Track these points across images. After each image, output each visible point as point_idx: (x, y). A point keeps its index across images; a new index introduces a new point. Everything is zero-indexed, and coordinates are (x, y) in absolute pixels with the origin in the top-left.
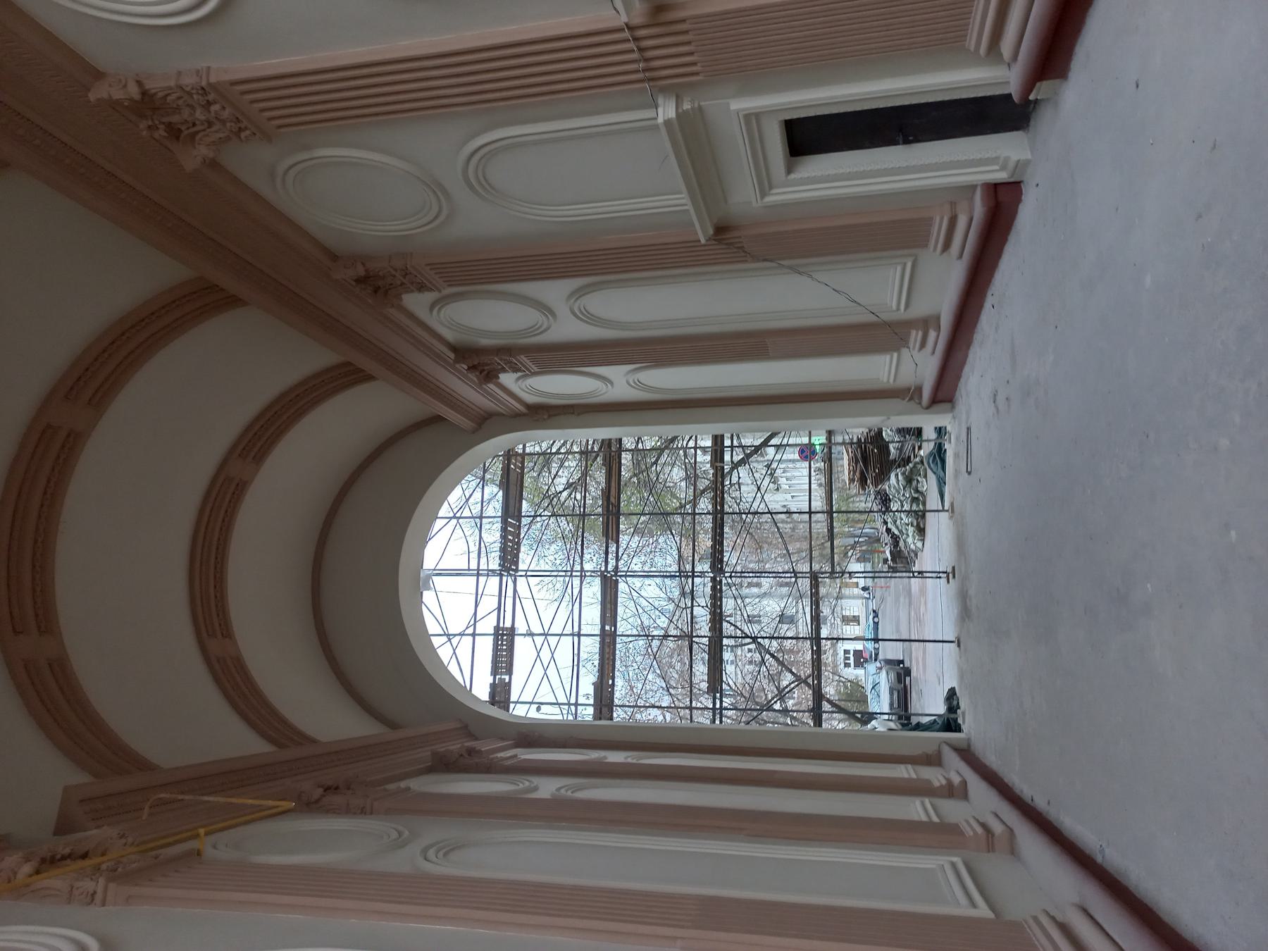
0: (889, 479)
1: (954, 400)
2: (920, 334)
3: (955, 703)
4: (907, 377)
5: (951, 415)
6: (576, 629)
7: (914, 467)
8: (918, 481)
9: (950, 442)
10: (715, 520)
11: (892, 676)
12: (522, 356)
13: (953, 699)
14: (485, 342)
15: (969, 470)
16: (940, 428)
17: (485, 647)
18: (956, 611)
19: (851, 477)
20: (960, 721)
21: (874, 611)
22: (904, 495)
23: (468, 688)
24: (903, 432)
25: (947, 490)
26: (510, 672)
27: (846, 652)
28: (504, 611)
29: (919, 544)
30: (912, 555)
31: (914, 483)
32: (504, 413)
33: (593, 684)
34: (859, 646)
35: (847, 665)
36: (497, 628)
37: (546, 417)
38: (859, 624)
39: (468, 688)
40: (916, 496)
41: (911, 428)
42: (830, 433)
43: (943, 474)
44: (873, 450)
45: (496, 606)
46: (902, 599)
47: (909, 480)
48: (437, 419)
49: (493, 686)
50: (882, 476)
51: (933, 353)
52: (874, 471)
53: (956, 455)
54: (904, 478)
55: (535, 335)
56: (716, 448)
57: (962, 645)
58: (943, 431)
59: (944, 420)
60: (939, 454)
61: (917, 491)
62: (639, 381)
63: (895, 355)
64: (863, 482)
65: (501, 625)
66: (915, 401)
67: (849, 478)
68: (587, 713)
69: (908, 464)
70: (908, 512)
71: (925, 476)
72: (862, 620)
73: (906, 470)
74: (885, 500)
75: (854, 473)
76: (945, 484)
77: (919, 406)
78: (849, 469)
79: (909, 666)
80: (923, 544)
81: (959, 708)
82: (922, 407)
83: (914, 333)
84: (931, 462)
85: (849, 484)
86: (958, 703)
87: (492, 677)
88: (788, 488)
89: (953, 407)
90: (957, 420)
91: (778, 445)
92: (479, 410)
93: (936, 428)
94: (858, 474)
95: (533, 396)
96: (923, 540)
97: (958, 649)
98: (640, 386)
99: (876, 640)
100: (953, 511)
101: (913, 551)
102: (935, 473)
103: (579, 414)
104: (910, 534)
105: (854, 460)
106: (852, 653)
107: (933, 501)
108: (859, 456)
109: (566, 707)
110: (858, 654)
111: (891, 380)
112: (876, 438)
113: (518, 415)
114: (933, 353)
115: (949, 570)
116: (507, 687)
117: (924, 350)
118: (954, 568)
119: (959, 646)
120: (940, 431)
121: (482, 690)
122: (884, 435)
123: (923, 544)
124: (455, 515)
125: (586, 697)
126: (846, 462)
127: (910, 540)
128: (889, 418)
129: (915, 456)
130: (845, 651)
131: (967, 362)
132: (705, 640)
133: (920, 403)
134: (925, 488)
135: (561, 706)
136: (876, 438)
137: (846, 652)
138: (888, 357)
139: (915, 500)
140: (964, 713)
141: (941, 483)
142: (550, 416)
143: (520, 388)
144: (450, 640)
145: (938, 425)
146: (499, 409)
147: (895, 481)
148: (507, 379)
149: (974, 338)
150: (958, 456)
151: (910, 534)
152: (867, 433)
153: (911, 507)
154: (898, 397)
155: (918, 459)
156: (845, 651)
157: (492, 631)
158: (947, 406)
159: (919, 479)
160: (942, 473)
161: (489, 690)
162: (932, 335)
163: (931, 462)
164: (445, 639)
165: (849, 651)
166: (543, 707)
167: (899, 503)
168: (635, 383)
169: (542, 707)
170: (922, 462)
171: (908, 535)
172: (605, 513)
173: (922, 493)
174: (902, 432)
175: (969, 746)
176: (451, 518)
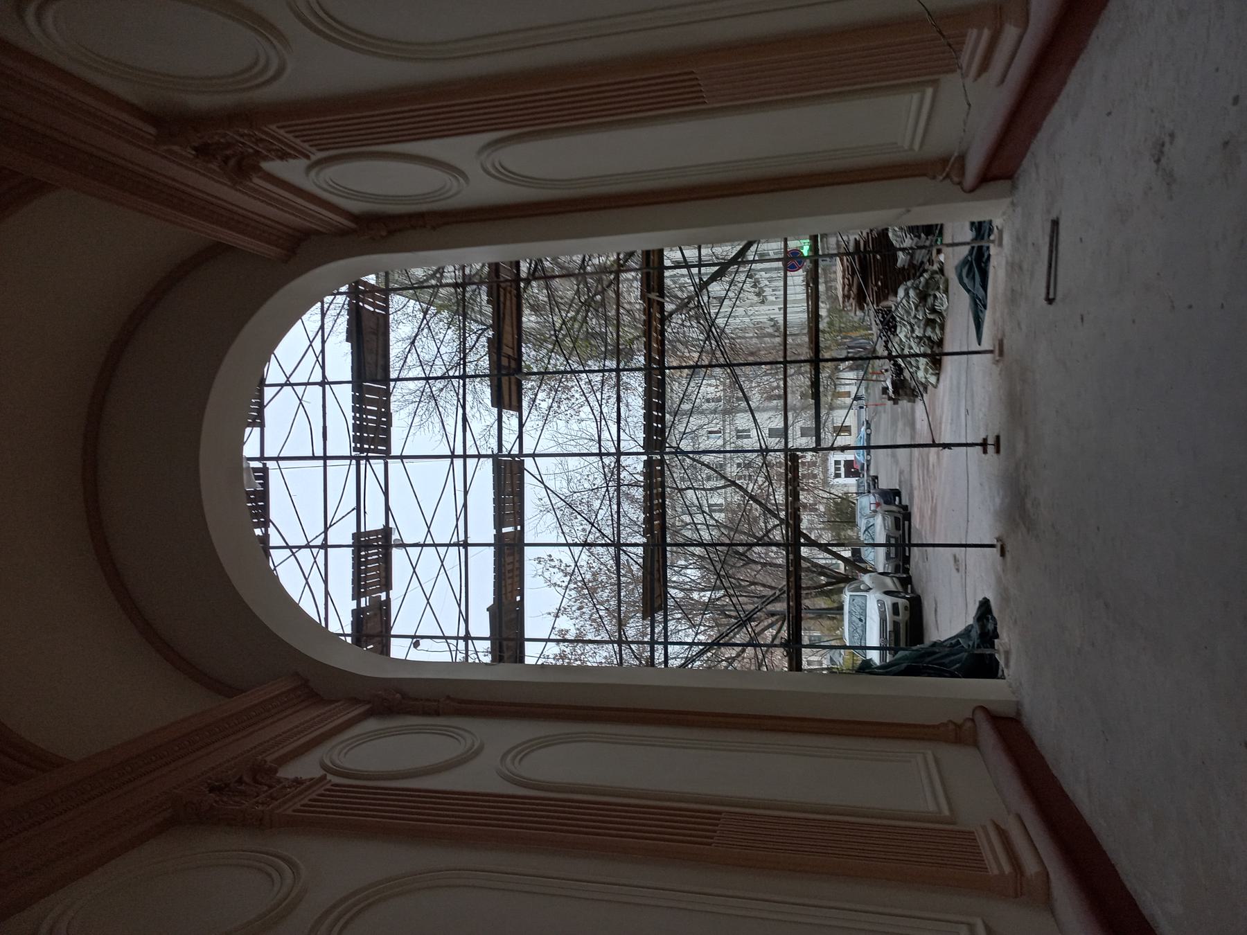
0: (896, 294)
1: (1016, 176)
2: (986, 33)
3: (990, 627)
4: (943, 140)
5: (1008, 201)
6: (462, 538)
7: (932, 278)
8: (935, 297)
9: (1000, 244)
10: (648, 379)
11: (890, 521)
12: (274, 127)
13: (988, 620)
14: (198, 101)
15: (1051, 296)
16: (980, 223)
17: (342, 563)
18: (998, 501)
19: (846, 293)
20: (1001, 659)
21: (867, 422)
22: (915, 317)
23: (323, 625)
24: (914, 230)
25: (988, 317)
26: (387, 585)
27: (837, 463)
28: (365, 512)
29: (933, 380)
30: (921, 389)
31: (930, 300)
32: (324, 231)
33: (488, 610)
34: (849, 455)
35: (837, 476)
36: (357, 536)
37: (384, 233)
38: (850, 435)
39: (323, 625)
40: (931, 317)
41: (937, 225)
42: (814, 239)
43: (983, 293)
44: (874, 257)
45: (354, 505)
46: (900, 425)
47: (923, 297)
48: (217, 250)
49: (357, 614)
50: (888, 289)
51: (1002, 81)
52: (876, 285)
53: (1015, 267)
54: (917, 295)
55: (258, 86)
56: (648, 270)
57: (1008, 556)
58: (986, 227)
59: (996, 212)
60: (977, 265)
61: (933, 311)
62: (502, 167)
63: (929, 91)
64: (861, 300)
65: (363, 530)
66: (951, 180)
67: (843, 295)
68: (482, 651)
69: (921, 275)
70: (920, 338)
71: (946, 291)
72: (854, 430)
73: (920, 282)
74: (889, 325)
75: (850, 286)
76: (985, 307)
77: (959, 187)
78: (843, 282)
79: (907, 504)
80: (938, 380)
81: (997, 637)
82: (965, 191)
83: (973, 33)
84: (964, 274)
85: (844, 302)
86: (995, 628)
87: (355, 601)
88: (775, 300)
89: (1014, 187)
90: (1019, 210)
91: (399, 381)
92: (285, 229)
93: (972, 224)
94: (854, 289)
95: (356, 202)
96: (938, 375)
97: (1001, 558)
98: (505, 175)
99: (868, 448)
100: (1001, 353)
101: (922, 384)
102: (968, 291)
103: (434, 228)
104: (922, 367)
105: (850, 272)
106: (843, 463)
107: (958, 332)
108: (857, 267)
109: (454, 642)
110: (849, 464)
111: (916, 147)
112: (881, 240)
113: (343, 233)
114: (1002, 80)
115: (991, 441)
116: (382, 611)
117: (985, 76)
118: (998, 438)
119: (1003, 553)
120: (981, 230)
121: (341, 622)
122: (890, 235)
123: (938, 380)
124: (288, 378)
125: (537, 561)
126: (840, 274)
127: (921, 374)
128: (909, 211)
129: (931, 262)
130: (835, 461)
131: (1061, 98)
132: (640, 550)
133: (960, 183)
134: (945, 307)
135: (449, 641)
136: (881, 240)
137: (837, 463)
138: (916, 97)
139: (930, 323)
140: (1007, 653)
141: (978, 306)
142: (391, 233)
143: (316, 185)
144: (293, 554)
145: (976, 219)
146: (308, 224)
147: (903, 298)
148: (291, 170)
149: (1093, 36)
150: (1021, 268)
151: (922, 367)
152: (868, 234)
153: (924, 332)
154: (924, 175)
155: (936, 267)
156: (835, 461)
157: (350, 542)
158: (1003, 185)
159: (938, 294)
160: (980, 292)
161: (351, 619)
162: (1010, 32)
163: (964, 274)
164: (287, 552)
165: (840, 461)
166: (422, 641)
167: (909, 327)
168: (494, 166)
169: (422, 641)
170: (941, 271)
171: (918, 368)
172: (496, 372)
173: (940, 314)
174: (915, 230)
175: (1019, 713)
176: (282, 385)
